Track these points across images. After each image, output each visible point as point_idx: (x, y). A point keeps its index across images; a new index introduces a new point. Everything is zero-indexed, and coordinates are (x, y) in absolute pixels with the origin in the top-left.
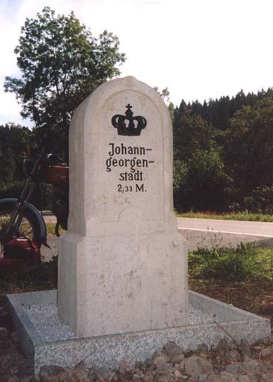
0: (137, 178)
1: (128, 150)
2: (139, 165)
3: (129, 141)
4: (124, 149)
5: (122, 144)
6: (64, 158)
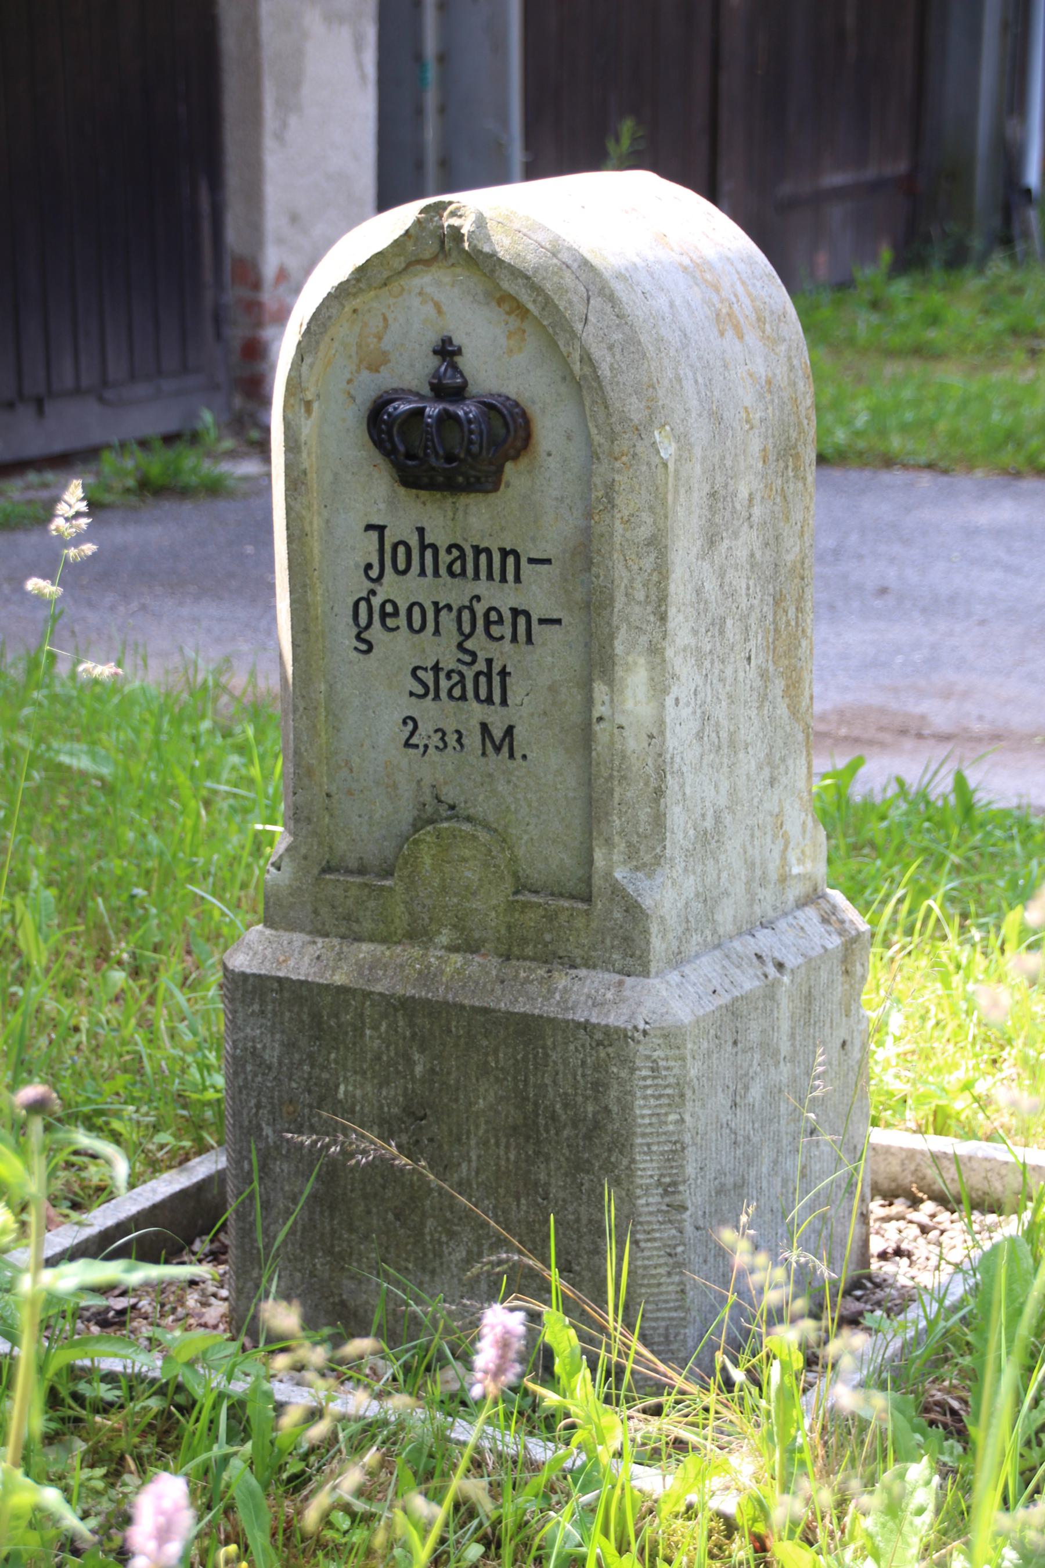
1: (444, 559)
2: (496, 631)
3: (441, 519)
4: (429, 554)
5: (421, 531)
6: (268, 999)
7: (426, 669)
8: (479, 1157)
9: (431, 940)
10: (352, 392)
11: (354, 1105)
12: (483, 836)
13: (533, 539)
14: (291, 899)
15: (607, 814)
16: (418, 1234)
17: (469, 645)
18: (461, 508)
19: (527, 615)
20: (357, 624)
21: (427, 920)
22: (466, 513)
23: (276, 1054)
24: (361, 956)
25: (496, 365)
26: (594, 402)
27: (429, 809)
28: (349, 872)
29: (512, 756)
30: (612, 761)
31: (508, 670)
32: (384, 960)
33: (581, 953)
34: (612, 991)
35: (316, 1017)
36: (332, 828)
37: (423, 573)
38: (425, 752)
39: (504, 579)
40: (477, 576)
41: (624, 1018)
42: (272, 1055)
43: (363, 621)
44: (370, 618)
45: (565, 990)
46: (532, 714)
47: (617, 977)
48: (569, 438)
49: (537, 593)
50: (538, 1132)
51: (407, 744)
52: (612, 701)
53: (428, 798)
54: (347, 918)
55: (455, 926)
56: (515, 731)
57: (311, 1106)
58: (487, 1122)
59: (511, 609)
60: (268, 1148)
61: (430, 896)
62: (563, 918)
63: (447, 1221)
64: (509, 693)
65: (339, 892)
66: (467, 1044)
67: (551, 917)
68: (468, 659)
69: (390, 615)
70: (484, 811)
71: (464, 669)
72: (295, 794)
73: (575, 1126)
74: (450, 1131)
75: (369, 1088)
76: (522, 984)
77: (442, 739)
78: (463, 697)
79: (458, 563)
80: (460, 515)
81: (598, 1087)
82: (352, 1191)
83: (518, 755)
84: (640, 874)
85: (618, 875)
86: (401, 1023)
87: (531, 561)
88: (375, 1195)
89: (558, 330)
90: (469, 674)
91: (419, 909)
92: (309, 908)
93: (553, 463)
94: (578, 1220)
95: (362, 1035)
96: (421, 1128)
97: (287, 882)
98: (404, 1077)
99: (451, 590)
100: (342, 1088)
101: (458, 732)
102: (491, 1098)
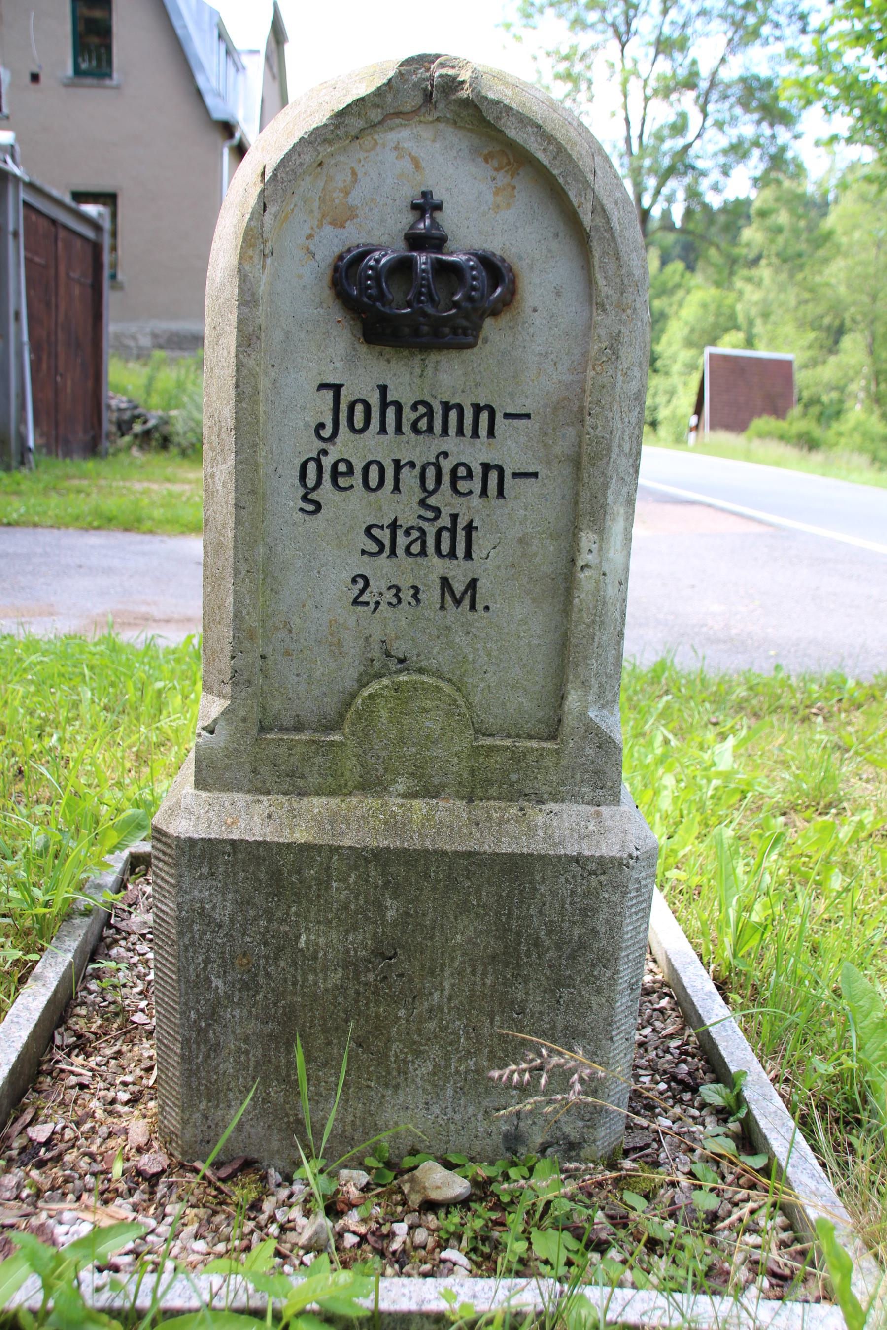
0: (445, 548)
1: (409, 415)
2: (462, 486)
3: (406, 379)
4: (391, 412)
5: (383, 389)
7: (382, 527)
8: (453, 985)
9: (385, 788)
10: (312, 248)
11: (316, 952)
12: (447, 688)
13: (512, 395)
14: (227, 761)
15: (586, 658)
16: (382, 1057)
17: (432, 501)
18: (431, 365)
19: (500, 470)
20: (305, 485)
21: (381, 771)
22: (436, 369)
23: (227, 912)
24: (316, 811)
25: (482, 217)
26: (604, 253)
27: (377, 665)
28: (283, 729)
29: (473, 607)
30: (596, 607)
31: (474, 524)
32: (343, 813)
33: (549, 789)
34: (593, 822)
35: (276, 877)
36: (265, 688)
37: (383, 430)
38: (375, 609)
39: (475, 434)
40: (445, 431)
41: (616, 848)
42: (223, 912)
43: (311, 481)
44: (318, 478)
45: (546, 826)
46: (499, 567)
47: (592, 809)
48: (558, 294)
49: (511, 448)
50: (519, 956)
51: (356, 602)
52: (601, 549)
53: (377, 653)
54: (291, 775)
55: (412, 774)
56: (478, 584)
57: (266, 957)
58: (463, 955)
59: (482, 464)
60: (219, 998)
61: (385, 748)
62: (531, 758)
63: (415, 1043)
64: (474, 547)
65: (283, 750)
66: (446, 886)
67: (518, 757)
68: (430, 515)
69: (343, 474)
70: (439, 662)
71: (425, 525)
72: (233, 657)
73: (559, 947)
74: (423, 967)
75: (334, 935)
76: (499, 824)
77: (396, 595)
78: (423, 553)
79: (425, 419)
80: (429, 371)
81: (587, 912)
82: (310, 1028)
83: (480, 606)
84: (605, 712)
85: (592, 714)
86: (372, 874)
87: (507, 416)
88: (337, 1029)
89: (569, 180)
90: (431, 531)
91: (373, 760)
92: (248, 768)
93: (538, 319)
94: (553, 1028)
95: (328, 888)
96: (390, 966)
97: (222, 745)
98: (375, 922)
99: (415, 447)
100: (303, 938)
101: (414, 587)
102: (470, 933)
